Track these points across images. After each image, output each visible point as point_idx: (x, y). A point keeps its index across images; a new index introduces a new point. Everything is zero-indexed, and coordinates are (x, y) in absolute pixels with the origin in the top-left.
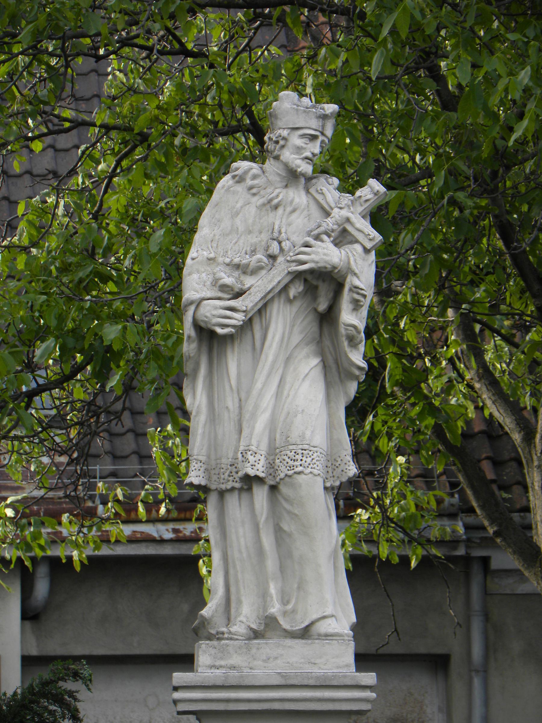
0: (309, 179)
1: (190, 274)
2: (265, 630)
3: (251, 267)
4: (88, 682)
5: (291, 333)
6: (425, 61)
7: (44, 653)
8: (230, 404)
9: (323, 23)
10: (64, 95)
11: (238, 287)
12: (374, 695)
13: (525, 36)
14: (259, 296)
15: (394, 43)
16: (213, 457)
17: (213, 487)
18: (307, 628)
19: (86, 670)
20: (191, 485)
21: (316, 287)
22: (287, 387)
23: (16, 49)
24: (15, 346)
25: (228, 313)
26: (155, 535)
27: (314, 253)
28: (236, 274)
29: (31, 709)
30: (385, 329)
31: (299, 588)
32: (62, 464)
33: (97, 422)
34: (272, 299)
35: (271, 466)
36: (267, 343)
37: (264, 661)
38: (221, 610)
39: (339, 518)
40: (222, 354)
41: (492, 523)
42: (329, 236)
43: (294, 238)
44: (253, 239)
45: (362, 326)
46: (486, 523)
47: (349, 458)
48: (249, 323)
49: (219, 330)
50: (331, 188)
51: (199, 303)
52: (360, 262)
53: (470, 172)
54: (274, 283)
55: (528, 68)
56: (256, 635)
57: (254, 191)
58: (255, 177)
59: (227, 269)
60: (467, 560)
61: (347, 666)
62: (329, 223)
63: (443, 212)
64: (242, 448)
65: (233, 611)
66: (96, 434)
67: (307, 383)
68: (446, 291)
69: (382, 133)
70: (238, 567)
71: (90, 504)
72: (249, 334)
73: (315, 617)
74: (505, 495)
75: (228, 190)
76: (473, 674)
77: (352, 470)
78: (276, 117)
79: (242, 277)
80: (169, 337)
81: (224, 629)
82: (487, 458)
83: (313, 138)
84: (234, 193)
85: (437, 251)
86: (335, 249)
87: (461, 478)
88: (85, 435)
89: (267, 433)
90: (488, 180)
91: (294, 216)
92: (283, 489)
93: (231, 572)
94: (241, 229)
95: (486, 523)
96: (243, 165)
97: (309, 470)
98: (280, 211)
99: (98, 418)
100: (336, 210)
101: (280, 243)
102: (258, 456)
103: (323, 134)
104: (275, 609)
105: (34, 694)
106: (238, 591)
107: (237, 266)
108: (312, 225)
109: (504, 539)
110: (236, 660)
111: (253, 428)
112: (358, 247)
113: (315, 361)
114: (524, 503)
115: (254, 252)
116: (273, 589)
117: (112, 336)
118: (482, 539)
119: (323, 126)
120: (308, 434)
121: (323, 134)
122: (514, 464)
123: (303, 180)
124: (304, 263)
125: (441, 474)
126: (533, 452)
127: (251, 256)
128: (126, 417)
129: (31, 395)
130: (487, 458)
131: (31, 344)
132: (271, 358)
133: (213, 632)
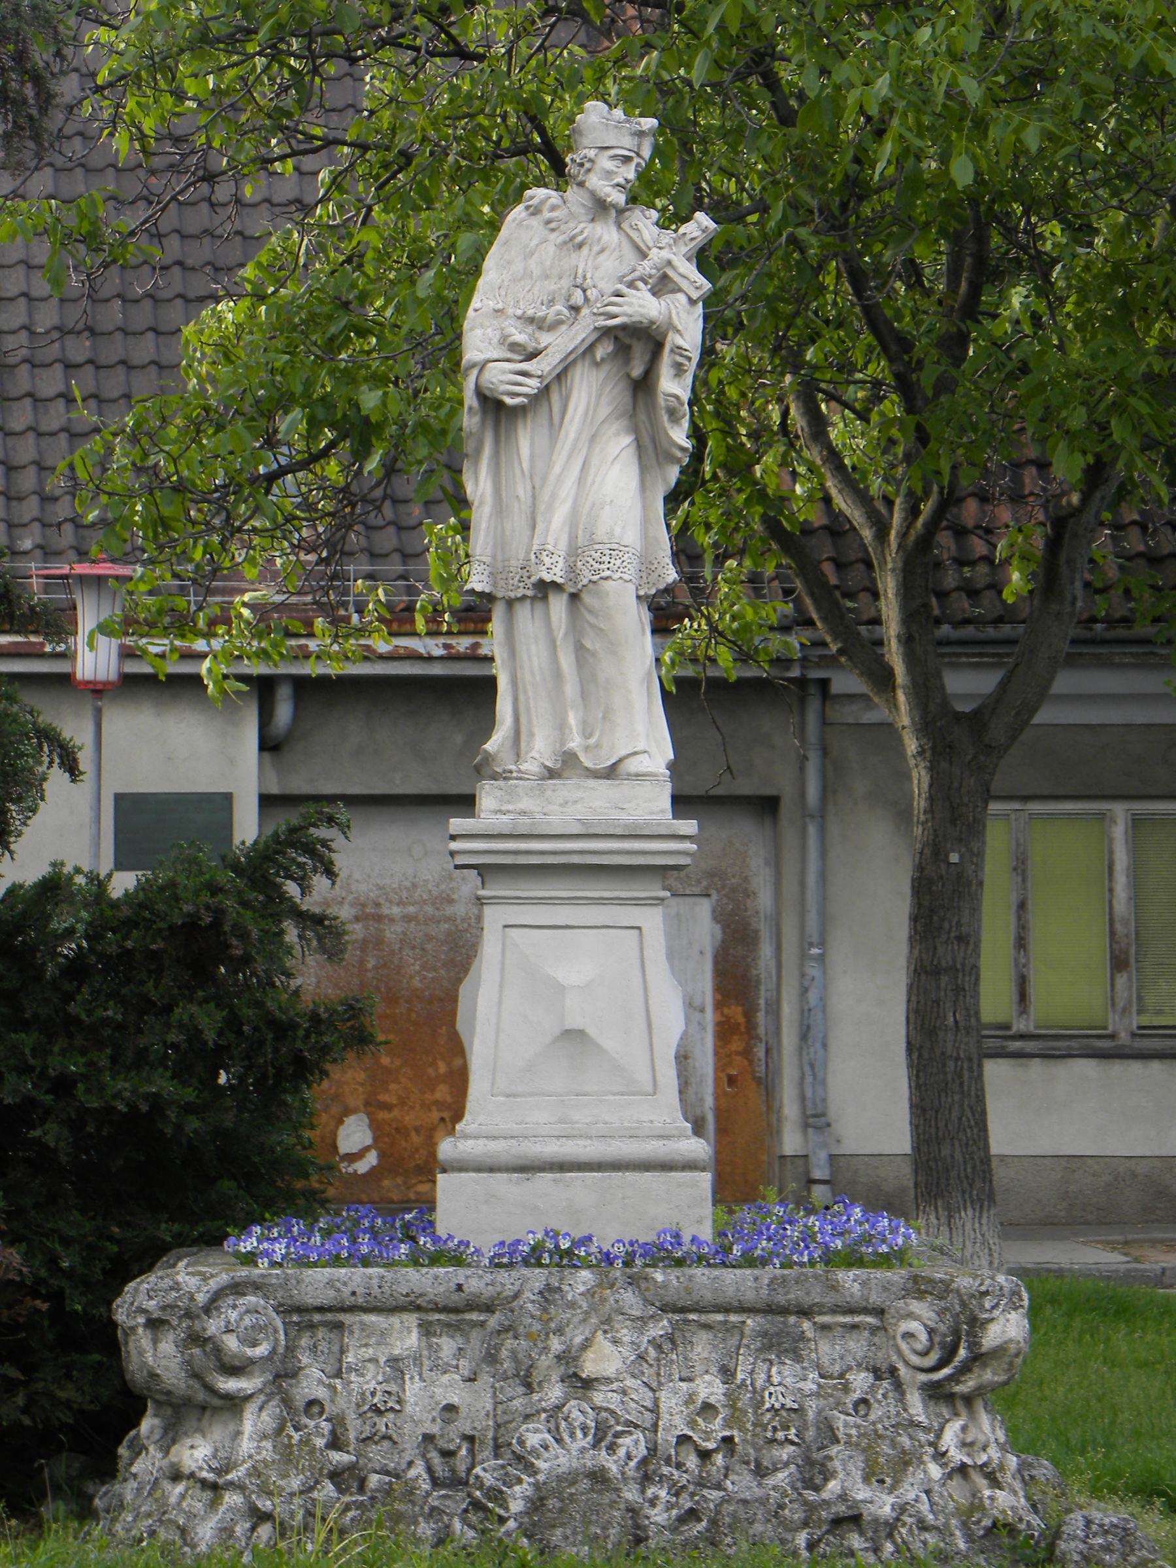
0: (620, 212)
1: (472, 329)
2: (562, 769)
3: (548, 321)
4: (344, 828)
5: (597, 404)
6: (758, 64)
7: (287, 792)
8: (521, 492)
9: (632, 18)
10: (311, 105)
11: (531, 346)
12: (695, 847)
13: (884, 34)
14: (559, 357)
15: (721, 42)
16: (499, 558)
17: (500, 595)
18: (614, 766)
19: (343, 813)
20: (472, 592)
21: (628, 348)
22: (593, 471)
23: (251, 48)
24: (253, 419)
25: (520, 378)
26: (422, 651)
27: (626, 303)
28: (530, 329)
29: (275, 861)
30: (707, 399)
31: (604, 718)
32: (309, 562)
33: (352, 513)
34: (574, 361)
35: (572, 569)
36: (568, 417)
37: (561, 805)
38: (509, 743)
39: (654, 632)
40: (512, 429)
41: (835, 640)
42: (646, 283)
43: (602, 285)
44: (551, 286)
45: (685, 395)
46: (828, 639)
47: (668, 560)
48: (545, 391)
49: (508, 401)
50: (648, 222)
51: (483, 365)
52: (683, 315)
53: (814, 203)
54: (577, 342)
55: (887, 75)
56: (552, 774)
57: (553, 225)
58: (553, 208)
59: (519, 323)
60: (802, 682)
61: (663, 811)
62: (646, 267)
63: (780, 253)
64: (535, 547)
65: (523, 744)
66: (350, 527)
67: (617, 467)
68: (783, 352)
69: (705, 152)
70: (530, 693)
71: (342, 612)
72: (546, 404)
73: (623, 753)
74: (850, 604)
75: (520, 224)
76: (808, 820)
77: (671, 575)
78: (580, 133)
79: (538, 334)
80: (440, 406)
81: (513, 767)
82: (829, 559)
83: (627, 160)
84: (528, 227)
85: (770, 301)
86: (653, 299)
87: (798, 584)
88: (338, 530)
89: (567, 529)
90: (837, 213)
91: (602, 257)
92: (586, 598)
93: (521, 697)
94: (536, 273)
95: (828, 639)
96: (538, 194)
97: (618, 575)
98: (585, 250)
99: (353, 508)
100: (655, 251)
101: (584, 291)
102: (555, 558)
103: (638, 155)
104: (575, 743)
105: (279, 843)
106: (530, 722)
107: (531, 320)
108: (625, 269)
109: (850, 659)
110: (526, 804)
111: (550, 522)
112: (681, 297)
113: (627, 439)
114: (872, 613)
115: (551, 302)
116: (572, 719)
117: (371, 404)
118: (821, 657)
119: (639, 146)
120: (618, 530)
121: (638, 155)
122: (861, 567)
123: (613, 213)
124: (615, 316)
125: (773, 579)
126: (887, 552)
127: (549, 307)
128: (388, 509)
129: (272, 478)
130: (829, 559)
131: (271, 417)
132: (572, 435)
133: (499, 770)
